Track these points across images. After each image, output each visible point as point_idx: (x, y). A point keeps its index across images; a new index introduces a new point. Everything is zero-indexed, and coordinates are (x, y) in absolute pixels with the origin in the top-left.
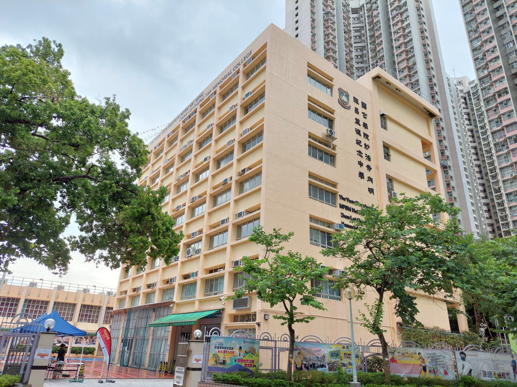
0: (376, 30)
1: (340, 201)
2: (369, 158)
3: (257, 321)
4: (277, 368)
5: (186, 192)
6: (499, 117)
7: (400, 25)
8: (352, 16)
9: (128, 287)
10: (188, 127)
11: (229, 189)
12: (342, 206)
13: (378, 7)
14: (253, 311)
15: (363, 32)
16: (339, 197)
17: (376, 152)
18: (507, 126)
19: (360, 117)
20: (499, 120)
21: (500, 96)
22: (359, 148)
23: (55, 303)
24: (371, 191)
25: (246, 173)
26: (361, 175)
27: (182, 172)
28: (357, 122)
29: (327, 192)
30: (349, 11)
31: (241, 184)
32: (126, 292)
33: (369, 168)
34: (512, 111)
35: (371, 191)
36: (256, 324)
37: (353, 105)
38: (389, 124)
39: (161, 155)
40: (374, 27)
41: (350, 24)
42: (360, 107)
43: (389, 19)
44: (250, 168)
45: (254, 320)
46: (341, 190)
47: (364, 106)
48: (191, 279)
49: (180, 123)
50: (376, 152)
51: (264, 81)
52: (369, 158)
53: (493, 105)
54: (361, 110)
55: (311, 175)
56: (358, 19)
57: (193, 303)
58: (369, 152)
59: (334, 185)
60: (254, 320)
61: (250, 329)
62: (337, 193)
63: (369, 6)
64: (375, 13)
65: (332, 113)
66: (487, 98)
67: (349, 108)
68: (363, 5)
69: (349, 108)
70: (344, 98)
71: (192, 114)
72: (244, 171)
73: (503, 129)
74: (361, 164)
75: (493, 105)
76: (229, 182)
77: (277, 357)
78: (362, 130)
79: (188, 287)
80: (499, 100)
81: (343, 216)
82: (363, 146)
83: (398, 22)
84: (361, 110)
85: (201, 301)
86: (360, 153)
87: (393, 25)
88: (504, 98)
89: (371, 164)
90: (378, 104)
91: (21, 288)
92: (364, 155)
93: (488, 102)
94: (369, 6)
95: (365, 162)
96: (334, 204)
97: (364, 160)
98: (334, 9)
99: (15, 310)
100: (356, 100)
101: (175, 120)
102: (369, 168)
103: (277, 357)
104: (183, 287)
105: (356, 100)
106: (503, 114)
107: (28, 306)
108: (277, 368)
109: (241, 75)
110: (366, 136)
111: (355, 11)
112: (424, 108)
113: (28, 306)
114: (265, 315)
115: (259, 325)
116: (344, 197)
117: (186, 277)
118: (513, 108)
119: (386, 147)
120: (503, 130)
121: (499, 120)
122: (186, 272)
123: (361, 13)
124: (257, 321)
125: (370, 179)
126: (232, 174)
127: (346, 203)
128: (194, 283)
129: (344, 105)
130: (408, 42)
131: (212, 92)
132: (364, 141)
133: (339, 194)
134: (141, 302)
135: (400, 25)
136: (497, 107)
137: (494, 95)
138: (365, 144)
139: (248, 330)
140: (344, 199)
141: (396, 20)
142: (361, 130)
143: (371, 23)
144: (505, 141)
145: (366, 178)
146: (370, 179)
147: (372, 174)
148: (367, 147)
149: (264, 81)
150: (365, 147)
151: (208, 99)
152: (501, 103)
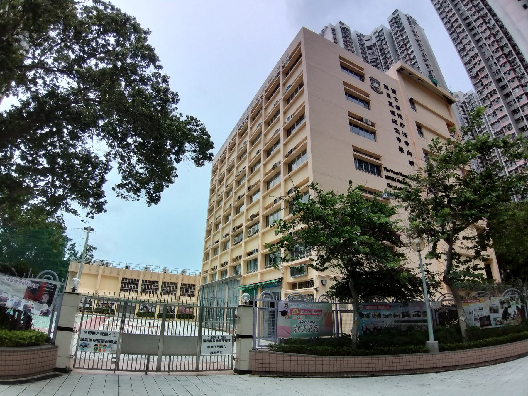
0: (388, 58)
1: (384, 173)
2: (405, 135)
3: (315, 287)
4: (340, 332)
5: (258, 202)
6: (494, 112)
7: (405, 53)
8: (368, 52)
9: (208, 268)
10: (242, 134)
11: (279, 173)
12: (387, 177)
13: (386, 42)
14: (309, 278)
15: (378, 62)
16: (383, 169)
17: (411, 130)
18: (501, 118)
19: (392, 100)
20: (494, 114)
21: (491, 96)
22: (395, 126)
23: (163, 282)
24: (412, 163)
25: (293, 153)
26: (401, 150)
27: (241, 169)
28: (391, 104)
29: (372, 165)
30: (365, 48)
31: (289, 167)
32: (207, 272)
33: (407, 143)
34: (502, 106)
35: (412, 163)
36: (313, 290)
37: (385, 91)
38: (417, 106)
39: (244, 181)
40: (386, 56)
41: (367, 57)
42: (390, 92)
43: (397, 50)
44: (295, 149)
45: (312, 286)
46: (385, 163)
47: (394, 92)
48: (254, 255)
49: (237, 131)
50: (411, 130)
51: (304, 103)
52: (405, 135)
53: (488, 103)
54: (392, 95)
55: (355, 149)
56: (373, 53)
57: (256, 275)
58: (405, 130)
59: (378, 158)
60: (312, 286)
61: (308, 295)
62: (381, 166)
63: (379, 42)
64: (385, 47)
65: (368, 96)
66: (483, 99)
67: (381, 93)
68: (375, 43)
69: (381, 93)
70: (376, 85)
71: (246, 121)
72: (290, 152)
73: (498, 121)
74: (399, 140)
75: (488, 103)
76: (278, 166)
77: (339, 321)
78: (396, 111)
79: (252, 264)
80: (492, 99)
81: (390, 186)
82: (399, 125)
83: (404, 50)
84: (392, 95)
85: (262, 274)
86: (397, 131)
87: (401, 53)
88: (495, 97)
89: (408, 140)
90: (405, 93)
91: (139, 272)
92: (401, 132)
93: (484, 101)
94: (379, 42)
95: (403, 139)
96: (379, 174)
97: (401, 136)
98: (353, 47)
99: (137, 288)
100: (386, 87)
101: (233, 131)
102: (407, 143)
103: (339, 321)
104: (248, 263)
105: (386, 87)
106: (497, 109)
107: (145, 285)
108: (340, 332)
109: (281, 75)
110: (400, 116)
111: (369, 48)
112: (443, 96)
113: (145, 285)
114: (322, 281)
115: (316, 290)
116: (388, 168)
117: (250, 254)
118: (503, 104)
119: (419, 127)
120: (499, 121)
121: (494, 114)
122: (249, 250)
123: (374, 49)
124: (315, 287)
125: (409, 153)
126: (280, 158)
127: (390, 174)
128: (256, 260)
129: (377, 90)
130: (414, 64)
131: (259, 98)
132: (399, 120)
133: (383, 166)
134: (218, 278)
135: (405, 53)
136: (491, 104)
137: (487, 96)
138: (400, 123)
139: (307, 296)
140: (388, 171)
141: (402, 49)
142: (395, 111)
143: (382, 55)
144: (502, 130)
145: (406, 153)
146: (409, 153)
147: (410, 148)
148: (402, 125)
149: (304, 103)
150: (401, 126)
151: (257, 104)
152: (493, 101)
